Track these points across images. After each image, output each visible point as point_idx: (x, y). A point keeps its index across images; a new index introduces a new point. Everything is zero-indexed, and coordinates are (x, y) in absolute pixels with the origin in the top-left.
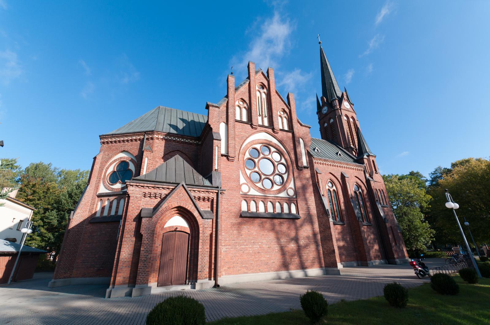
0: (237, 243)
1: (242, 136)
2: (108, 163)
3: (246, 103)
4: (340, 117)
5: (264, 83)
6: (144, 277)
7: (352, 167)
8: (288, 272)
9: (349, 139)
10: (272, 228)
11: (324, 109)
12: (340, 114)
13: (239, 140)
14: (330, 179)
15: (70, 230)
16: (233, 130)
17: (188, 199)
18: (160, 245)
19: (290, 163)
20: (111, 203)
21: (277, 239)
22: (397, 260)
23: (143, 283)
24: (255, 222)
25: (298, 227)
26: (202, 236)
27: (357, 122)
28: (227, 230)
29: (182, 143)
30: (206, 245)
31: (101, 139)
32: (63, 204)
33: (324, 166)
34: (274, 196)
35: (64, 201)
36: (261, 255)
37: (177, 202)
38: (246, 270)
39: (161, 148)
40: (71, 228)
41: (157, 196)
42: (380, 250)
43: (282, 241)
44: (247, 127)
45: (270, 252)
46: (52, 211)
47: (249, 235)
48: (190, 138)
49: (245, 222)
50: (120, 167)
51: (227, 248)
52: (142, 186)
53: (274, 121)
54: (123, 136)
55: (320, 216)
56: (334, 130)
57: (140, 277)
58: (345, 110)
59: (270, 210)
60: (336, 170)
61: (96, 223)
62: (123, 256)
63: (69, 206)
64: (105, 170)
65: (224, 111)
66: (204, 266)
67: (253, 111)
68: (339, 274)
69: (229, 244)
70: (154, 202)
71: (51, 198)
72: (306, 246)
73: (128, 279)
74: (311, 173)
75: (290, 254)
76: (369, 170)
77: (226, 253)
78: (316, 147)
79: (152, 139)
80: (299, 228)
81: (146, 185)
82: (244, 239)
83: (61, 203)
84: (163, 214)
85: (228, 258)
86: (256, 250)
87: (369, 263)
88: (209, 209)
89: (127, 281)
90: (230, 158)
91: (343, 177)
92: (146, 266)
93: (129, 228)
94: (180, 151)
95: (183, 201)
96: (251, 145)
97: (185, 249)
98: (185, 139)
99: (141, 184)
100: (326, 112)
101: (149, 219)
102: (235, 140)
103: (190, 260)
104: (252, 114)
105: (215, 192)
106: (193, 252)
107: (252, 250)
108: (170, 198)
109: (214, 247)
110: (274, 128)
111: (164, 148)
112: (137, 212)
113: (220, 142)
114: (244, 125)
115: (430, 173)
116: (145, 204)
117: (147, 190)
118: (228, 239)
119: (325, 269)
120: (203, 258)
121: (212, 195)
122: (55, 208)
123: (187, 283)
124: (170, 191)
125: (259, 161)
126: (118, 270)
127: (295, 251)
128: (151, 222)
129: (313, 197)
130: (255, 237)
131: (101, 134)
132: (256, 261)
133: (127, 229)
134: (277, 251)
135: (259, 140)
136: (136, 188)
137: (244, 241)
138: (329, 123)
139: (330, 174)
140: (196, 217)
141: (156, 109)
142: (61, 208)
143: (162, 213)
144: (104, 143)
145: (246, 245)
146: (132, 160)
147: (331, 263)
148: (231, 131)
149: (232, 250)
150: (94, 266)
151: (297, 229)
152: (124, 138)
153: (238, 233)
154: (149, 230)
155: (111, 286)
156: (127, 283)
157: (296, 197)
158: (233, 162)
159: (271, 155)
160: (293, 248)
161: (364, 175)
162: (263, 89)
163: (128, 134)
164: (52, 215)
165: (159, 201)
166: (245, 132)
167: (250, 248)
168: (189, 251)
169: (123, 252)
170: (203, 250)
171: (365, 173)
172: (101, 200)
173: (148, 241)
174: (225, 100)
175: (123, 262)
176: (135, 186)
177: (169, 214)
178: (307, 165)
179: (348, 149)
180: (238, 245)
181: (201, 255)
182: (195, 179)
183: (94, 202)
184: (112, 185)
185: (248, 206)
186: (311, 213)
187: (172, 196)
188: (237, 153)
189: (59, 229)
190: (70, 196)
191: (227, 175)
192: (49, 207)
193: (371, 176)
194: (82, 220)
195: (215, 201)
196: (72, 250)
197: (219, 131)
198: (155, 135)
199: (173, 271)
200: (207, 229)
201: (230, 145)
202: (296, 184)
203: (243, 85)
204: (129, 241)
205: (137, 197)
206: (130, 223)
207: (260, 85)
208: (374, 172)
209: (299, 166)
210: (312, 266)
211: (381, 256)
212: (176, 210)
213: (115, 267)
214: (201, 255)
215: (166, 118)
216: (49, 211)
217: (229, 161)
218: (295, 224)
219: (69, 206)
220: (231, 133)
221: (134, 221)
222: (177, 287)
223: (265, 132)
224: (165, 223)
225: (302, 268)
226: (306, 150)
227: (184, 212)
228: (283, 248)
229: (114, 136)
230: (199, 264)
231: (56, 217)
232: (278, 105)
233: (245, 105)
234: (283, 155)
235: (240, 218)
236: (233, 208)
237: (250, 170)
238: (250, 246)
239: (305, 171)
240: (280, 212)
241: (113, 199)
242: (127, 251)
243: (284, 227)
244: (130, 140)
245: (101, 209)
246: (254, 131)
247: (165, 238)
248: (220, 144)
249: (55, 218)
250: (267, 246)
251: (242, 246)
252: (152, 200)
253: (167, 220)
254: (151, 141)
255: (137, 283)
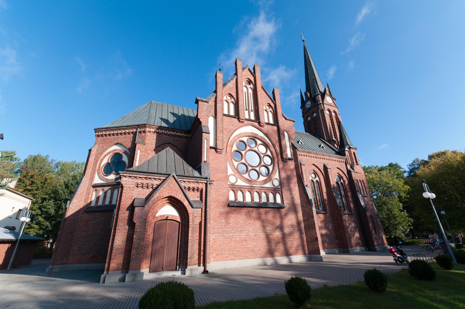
0: (225, 231)
1: (230, 129)
2: (102, 155)
3: (234, 98)
4: (323, 111)
5: (250, 79)
6: (137, 264)
7: (334, 159)
8: (274, 259)
9: (331, 132)
10: (258, 217)
11: (308, 104)
12: (323, 108)
13: (227, 134)
14: (313, 171)
15: (66, 219)
16: (221, 123)
17: (179, 189)
18: (151, 233)
19: (275, 155)
20: (105, 193)
21: (263, 227)
22: (377, 247)
23: (136, 269)
24: (242, 211)
25: (283, 216)
26: (192, 225)
27: (338, 116)
28: (215, 219)
29: (172, 136)
30: (195, 233)
31: (95, 132)
32: (60, 194)
33: (308, 157)
34: (260, 186)
35: (60, 191)
36: (247, 243)
37: (168, 192)
38: (234, 257)
39: (153, 141)
40: (68, 217)
41: (149, 186)
42: (360, 238)
43: (268, 229)
44: (234, 121)
45: (256, 240)
46: (50, 201)
47: (236, 224)
48: (180, 131)
49: (232, 211)
50: (114, 159)
51: (215, 236)
52: (134, 177)
53: (260, 115)
54: (117, 129)
55: (303, 205)
56: (317, 124)
57: (133, 263)
58: (327, 104)
59: (257, 200)
60: (319, 161)
61: (91, 212)
62: (116, 243)
63: (66, 196)
64: (100, 162)
65: (213, 106)
66: (194, 253)
67: (240, 106)
68: (322, 261)
69: (218, 232)
70: (146, 192)
71: (48, 189)
72: (291, 234)
73: (122, 265)
74: (295, 165)
75: (275, 242)
76: (350, 161)
77: (214, 240)
78: (299, 139)
79: (144, 132)
80: (284, 217)
81: (138, 176)
82: (232, 228)
83: (58, 193)
84: (155, 204)
85: (216, 245)
86: (243, 237)
87: (350, 250)
88: (199, 199)
89: (121, 268)
90: (218, 150)
91: (325, 168)
92: (138, 253)
93: (122, 217)
94: (171, 144)
95: (174, 191)
96: (239, 138)
97: (175, 236)
98: (176, 132)
99: (134, 175)
100: (309, 107)
101: (141, 208)
102: (223, 133)
103: (181, 247)
104: (240, 109)
105: (204, 183)
106: (183, 240)
107: (239, 238)
108: (161, 189)
109: (203, 235)
110: (260, 121)
111: (156, 141)
112: (130, 202)
113: (209, 135)
114: (232, 119)
115: (408, 165)
116: (138, 194)
117: (139, 181)
118: (216, 227)
119: (309, 256)
120: (193, 245)
121: (201, 186)
122: (52, 198)
123: (178, 269)
124: (161, 181)
125: (246, 153)
126: (112, 257)
127: (280, 238)
128: (143, 211)
129: (297, 188)
130: (242, 226)
131: (96, 128)
132: (243, 248)
133: (121, 218)
134: (263, 238)
135: (245, 133)
136: (129, 179)
137: (231, 229)
138: (312, 117)
139: (313, 165)
140: (186, 206)
141: (148, 104)
142: (58, 198)
143: (154, 203)
144: (98, 136)
145: (234, 233)
146: (125, 152)
147: (314, 250)
148: (219, 125)
149: (220, 237)
150: (89, 253)
151: (282, 218)
152: (118, 131)
153: (226, 221)
154: (141, 219)
155: (105, 272)
156: (120, 269)
157: (281, 187)
158: (221, 154)
159: (257, 147)
160: (278, 236)
161: (345, 166)
162: (250, 84)
163: (121, 128)
164: (49, 204)
165: (151, 191)
166: (233, 126)
167: (238, 236)
168: (180, 238)
169: (117, 240)
170: (192, 238)
171: (346, 165)
172: (96, 190)
173: (140, 229)
174: (214, 95)
175: (116, 249)
176: (128, 177)
177: (161, 204)
178: (292, 157)
179: (331, 142)
180: (226, 233)
181: (191, 242)
182: (185, 171)
183: (89, 192)
184: (106, 176)
185: (235, 196)
186: (295, 202)
187: (163, 186)
188: (225, 145)
189: (56, 218)
190: (67, 186)
191: (216, 166)
192: (47, 196)
193: (352, 167)
194: (77, 209)
195: (204, 191)
196: (69, 237)
197: (208, 124)
198: (147, 129)
199: (164, 258)
200: (196, 218)
201: (219, 138)
202: (281, 175)
203: (231, 81)
204: (123, 229)
205: (130, 187)
206: (123, 212)
207: (247, 81)
208: (355, 163)
209: (284, 158)
210: (296, 253)
211: (362, 243)
212: (167, 200)
213: (110, 254)
214: (191, 242)
215: (157, 112)
216: (47, 200)
217: (217, 153)
218: (280, 213)
219: (66, 196)
220: (219, 126)
221: (127, 210)
222: (168, 273)
223: (252, 126)
224: (157, 212)
225: (287, 255)
226: (290, 143)
227: (175, 202)
228: (269, 236)
229: (108, 129)
230: (189, 251)
231: (53, 206)
232: (264, 100)
233: (233, 100)
234: (268, 147)
235: (227, 208)
236: (221, 198)
237: (237, 161)
238: (238, 234)
239: (289, 162)
240: (266, 201)
241: (108, 189)
242: (121, 239)
243: (270, 216)
244: (124, 133)
245: (96, 199)
246: (242, 124)
247: (157, 226)
248: (209, 137)
249: (52, 207)
250: (254, 234)
251: (230, 234)
252: (145, 190)
253: (158, 209)
254: (143, 134)
255: (130, 269)
